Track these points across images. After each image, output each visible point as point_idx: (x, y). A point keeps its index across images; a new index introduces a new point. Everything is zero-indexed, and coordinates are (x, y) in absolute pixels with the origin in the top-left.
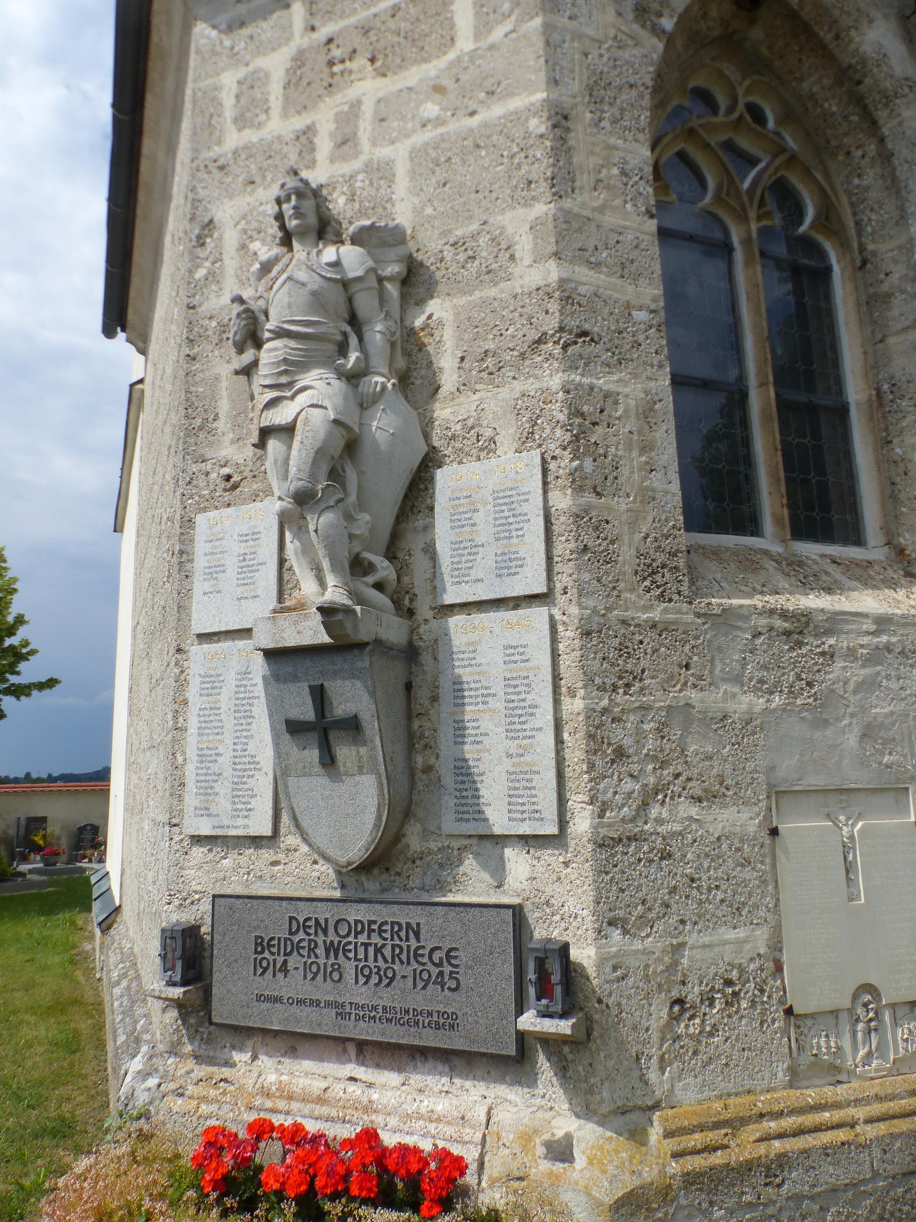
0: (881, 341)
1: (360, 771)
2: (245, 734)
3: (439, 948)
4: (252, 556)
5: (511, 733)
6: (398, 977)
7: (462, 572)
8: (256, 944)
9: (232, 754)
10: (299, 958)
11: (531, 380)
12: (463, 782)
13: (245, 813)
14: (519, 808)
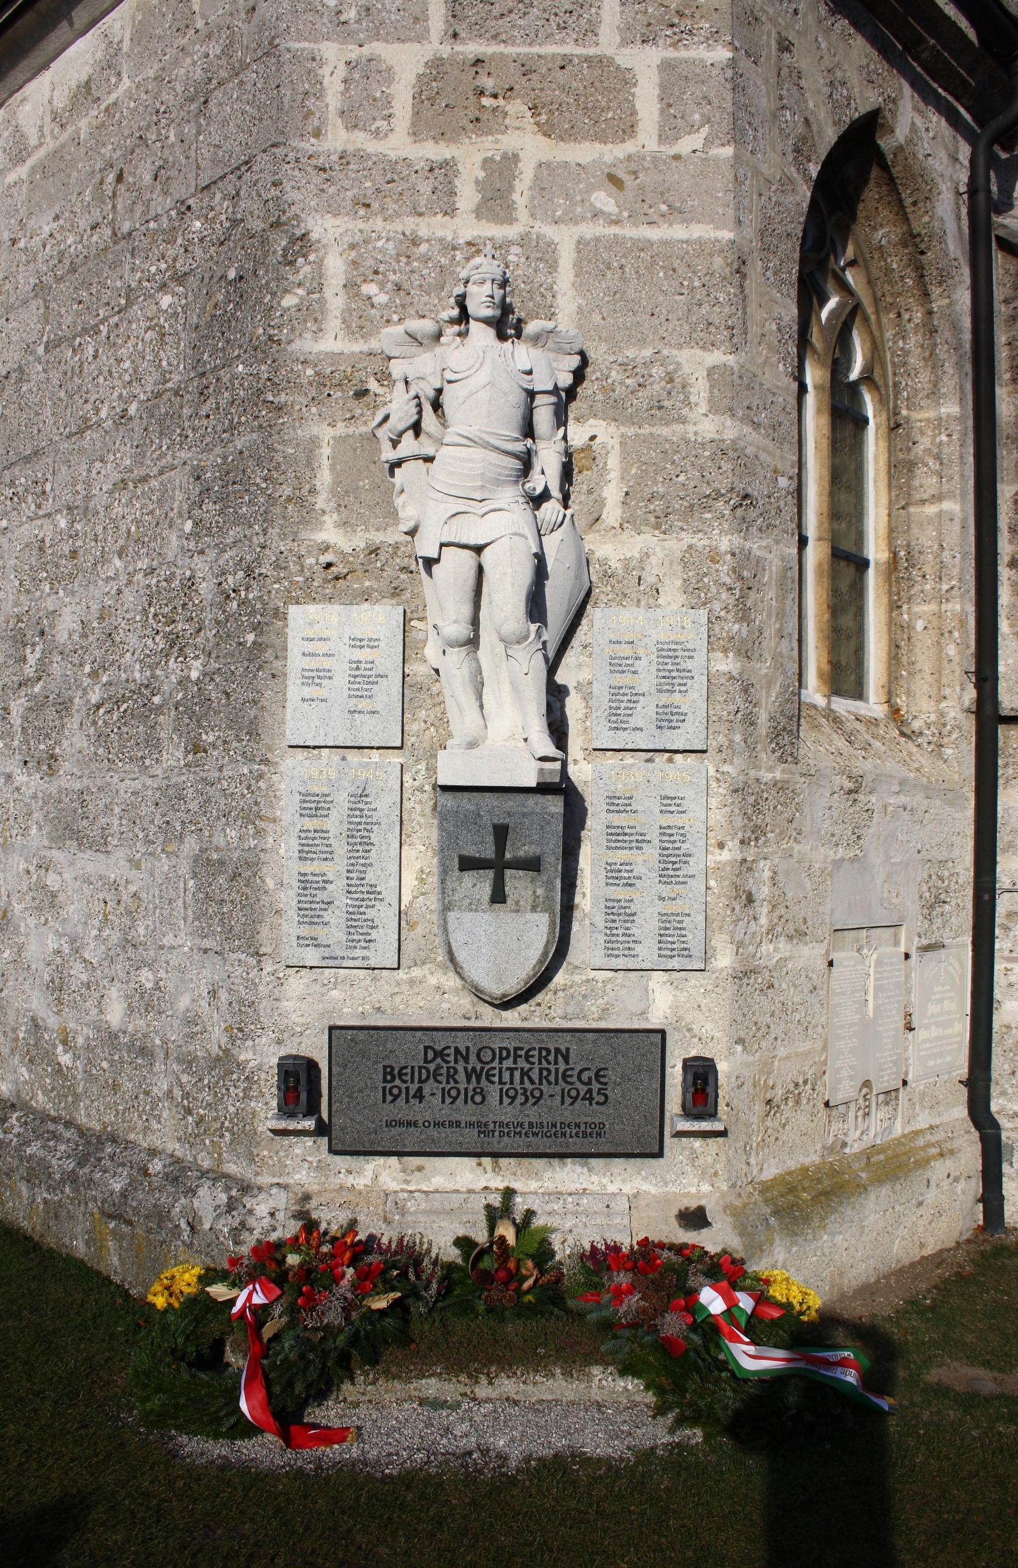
0: (903, 508)
1: (534, 909)
2: (362, 861)
3: (588, 1069)
4: (369, 666)
5: (664, 878)
6: (545, 1096)
7: (621, 718)
8: (385, 1074)
9: (346, 881)
10: (436, 1085)
11: (700, 535)
12: (614, 921)
13: (363, 944)
14: (669, 946)
